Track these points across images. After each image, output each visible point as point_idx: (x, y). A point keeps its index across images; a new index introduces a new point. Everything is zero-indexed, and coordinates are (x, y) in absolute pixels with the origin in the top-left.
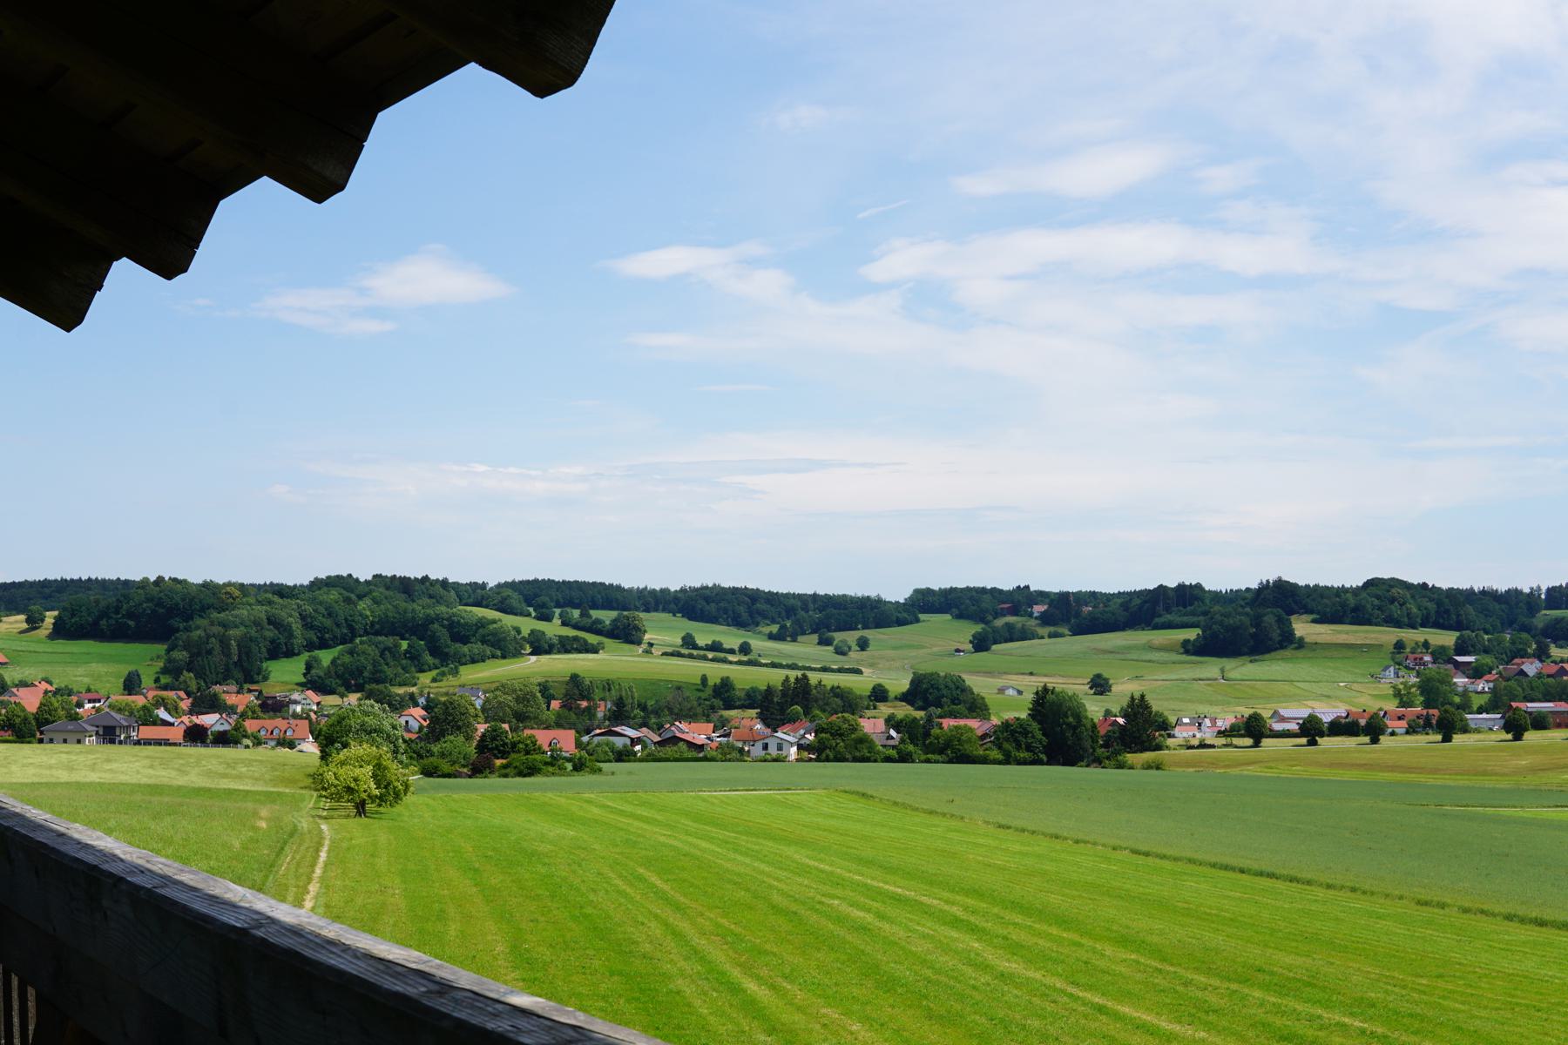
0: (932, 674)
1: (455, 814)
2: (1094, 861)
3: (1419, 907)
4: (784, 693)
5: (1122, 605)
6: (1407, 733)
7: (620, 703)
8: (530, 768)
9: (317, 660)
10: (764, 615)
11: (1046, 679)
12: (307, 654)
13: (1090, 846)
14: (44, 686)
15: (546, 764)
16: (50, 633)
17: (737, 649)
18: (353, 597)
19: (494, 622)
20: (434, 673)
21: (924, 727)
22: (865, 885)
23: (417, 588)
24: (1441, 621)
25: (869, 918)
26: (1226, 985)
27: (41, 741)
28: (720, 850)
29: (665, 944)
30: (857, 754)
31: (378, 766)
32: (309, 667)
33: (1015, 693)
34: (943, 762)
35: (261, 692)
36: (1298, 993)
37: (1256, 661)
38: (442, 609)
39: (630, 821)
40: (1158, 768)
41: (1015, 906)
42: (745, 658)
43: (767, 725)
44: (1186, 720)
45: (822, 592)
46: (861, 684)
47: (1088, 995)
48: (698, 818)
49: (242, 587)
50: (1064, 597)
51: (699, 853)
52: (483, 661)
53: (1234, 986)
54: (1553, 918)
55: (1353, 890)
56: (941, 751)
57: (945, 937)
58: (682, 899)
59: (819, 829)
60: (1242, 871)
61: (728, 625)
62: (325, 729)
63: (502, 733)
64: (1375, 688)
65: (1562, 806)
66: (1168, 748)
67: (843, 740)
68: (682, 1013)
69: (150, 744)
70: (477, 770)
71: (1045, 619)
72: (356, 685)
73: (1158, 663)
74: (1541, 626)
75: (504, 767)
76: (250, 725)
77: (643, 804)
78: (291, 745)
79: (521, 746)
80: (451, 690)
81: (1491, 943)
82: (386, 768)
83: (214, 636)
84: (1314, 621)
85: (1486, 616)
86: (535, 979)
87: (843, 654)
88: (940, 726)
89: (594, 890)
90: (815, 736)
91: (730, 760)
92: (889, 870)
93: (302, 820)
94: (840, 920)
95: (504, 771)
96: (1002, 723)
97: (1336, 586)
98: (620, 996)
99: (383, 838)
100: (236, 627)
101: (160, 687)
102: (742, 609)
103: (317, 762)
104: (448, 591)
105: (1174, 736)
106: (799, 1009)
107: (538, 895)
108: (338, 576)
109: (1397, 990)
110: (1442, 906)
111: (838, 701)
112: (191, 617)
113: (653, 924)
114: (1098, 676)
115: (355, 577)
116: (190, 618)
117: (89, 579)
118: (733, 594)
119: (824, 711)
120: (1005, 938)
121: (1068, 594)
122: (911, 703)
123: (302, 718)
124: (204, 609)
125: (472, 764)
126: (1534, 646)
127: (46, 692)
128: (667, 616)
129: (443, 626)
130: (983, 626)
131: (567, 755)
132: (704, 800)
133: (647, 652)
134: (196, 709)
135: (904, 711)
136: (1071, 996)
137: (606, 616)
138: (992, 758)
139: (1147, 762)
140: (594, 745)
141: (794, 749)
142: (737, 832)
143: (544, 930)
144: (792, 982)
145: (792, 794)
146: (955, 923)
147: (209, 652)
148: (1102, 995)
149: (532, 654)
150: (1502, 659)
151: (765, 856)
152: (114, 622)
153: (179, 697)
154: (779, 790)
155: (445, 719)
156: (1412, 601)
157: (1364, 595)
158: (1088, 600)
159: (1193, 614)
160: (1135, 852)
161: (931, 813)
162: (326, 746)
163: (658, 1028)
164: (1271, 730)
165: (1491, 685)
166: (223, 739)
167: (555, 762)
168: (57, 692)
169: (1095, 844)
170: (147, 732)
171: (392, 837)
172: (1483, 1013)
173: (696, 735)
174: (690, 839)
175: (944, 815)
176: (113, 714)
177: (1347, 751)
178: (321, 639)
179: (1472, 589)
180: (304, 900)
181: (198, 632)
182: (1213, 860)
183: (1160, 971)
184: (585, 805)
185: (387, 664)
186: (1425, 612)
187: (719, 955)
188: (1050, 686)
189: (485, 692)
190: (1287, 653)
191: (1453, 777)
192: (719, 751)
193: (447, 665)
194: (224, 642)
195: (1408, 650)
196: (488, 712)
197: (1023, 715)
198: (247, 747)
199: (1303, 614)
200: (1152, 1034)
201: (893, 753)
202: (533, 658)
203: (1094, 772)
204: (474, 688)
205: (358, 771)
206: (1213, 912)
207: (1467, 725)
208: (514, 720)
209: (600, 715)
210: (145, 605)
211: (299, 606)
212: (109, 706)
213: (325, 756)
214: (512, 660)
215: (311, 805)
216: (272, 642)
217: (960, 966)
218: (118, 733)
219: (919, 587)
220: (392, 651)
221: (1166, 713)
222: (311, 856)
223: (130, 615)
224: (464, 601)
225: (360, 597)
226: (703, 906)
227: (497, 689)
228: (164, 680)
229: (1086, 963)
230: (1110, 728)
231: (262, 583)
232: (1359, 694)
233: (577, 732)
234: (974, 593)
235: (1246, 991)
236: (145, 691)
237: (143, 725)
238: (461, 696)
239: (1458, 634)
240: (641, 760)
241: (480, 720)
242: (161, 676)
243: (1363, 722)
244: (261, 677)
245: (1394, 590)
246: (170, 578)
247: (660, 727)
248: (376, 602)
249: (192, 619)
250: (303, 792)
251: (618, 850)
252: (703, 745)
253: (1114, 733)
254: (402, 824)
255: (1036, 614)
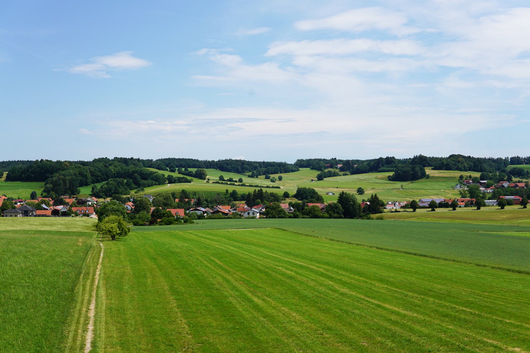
0: (304, 188)
1: (145, 238)
2: (365, 252)
3: (477, 267)
4: (254, 195)
5: (367, 164)
6: (465, 207)
7: (199, 199)
8: (169, 222)
9: (95, 186)
10: (246, 169)
11: (343, 190)
12: (92, 185)
13: (362, 246)
14: (4, 197)
15: (175, 220)
16: (5, 179)
17: (238, 181)
18: (108, 165)
19: (155, 173)
20: (136, 190)
21: (302, 206)
22: (289, 262)
23: (129, 162)
24: (475, 169)
25: (293, 274)
26: (420, 296)
27: (3, 216)
28: (237, 250)
29: (224, 285)
30: (280, 216)
31: (119, 223)
32: (93, 189)
33: (332, 194)
34: (309, 218)
35: (77, 198)
36: (445, 299)
37: (413, 183)
38: (138, 168)
39: (205, 240)
40: (381, 219)
41: (342, 268)
42: (241, 184)
43: (249, 206)
44: (390, 203)
45: (266, 161)
46: (280, 192)
47: (373, 301)
48: (229, 238)
49: (70, 162)
50: (348, 161)
51: (230, 251)
52: (152, 186)
53: (423, 297)
54: (524, 270)
55: (454, 261)
56: (308, 214)
57: (320, 280)
58: (228, 268)
59: (270, 242)
60: (415, 255)
61: (235, 173)
62: (99, 210)
63: (159, 210)
64: (453, 192)
65: (519, 231)
66: (384, 212)
67: (275, 211)
68: (233, 310)
69: (40, 216)
70: (152, 223)
71: (342, 169)
72: (109, 195)
73: (380, 183)
74: (509, 170)
75: (160, 222)
76: (74, 209)
77: (209, 234)
78: (88, 215)
79: (166, 215)
80: (142, 196)
81: (505, 279)
82: (122, 224)
83: (61, 179)
84: (432, 169)
85: (490, 167)
86: (180, 299)
87: (274, 182)
88: (307, 206)
89: (197, 266)
90: (265, 210)
91: (237, 218)
92: (297, 256)
93: (94, 242)
94: (283, 274)
95: (160, 223)
96: (328, 204)
97: (439, 157)
98: (210, 304)
99: (122, 248)
100: (68, 176)
101: (43, 197)
102: (239, 167)
103: (97, 221)
104: (140, 163)
105: (386, 208)
106: (274, 308)
107: (177, 268)
108: (102, 158)
109: (478, 297)
110: (485, 266)
111: (273, 198)
112: (53, 173)
113: (219, 277)
114: (360, 188)
115: (108, 158)
116: (52, 173)
117: (18, 161)
118: (236, 162)
119: (268, 201)
120: (340, 280)
121: (349, 160)
122: (297, 198)
123: (91, 206)
124: (57, 170)
125: (150, 221)
126: (507, 177)
127: (4, 199)
128: (214, 170)
129: (139, 175)
130: (321, 172)
131: (182, 217)
132: (229, 232)
133: (208, 182)
134: (55, 204)
135: (295, 201)
136: (367, 301)
137: (193, 170)
138: (325, 216)
139: (378, 217)
140: (190, 214)
141: (258, 214)
142: (242, 243)
143: (181, 280)
144: (270, 298)
145: (260, 230)
146: (322, 275)
147: (59, 185)
148: (378, 300)
149: (169, 183)
150: (496, 182)
151: (253, 252)
152: (27, 175)
153: (49, 200)
154: (255, 228)
155: (140, 206)
156: (465, 162)
157: (449, 160)
158: (356, 163)
159: (392, 167)
160: (377, 248)
161: (307, 235)
162: (100, 216)
163: (225, 316)
164: (419, 206)
165: (492, 190)
166: (65, 214)
167: (178, 220)
168: (8, 199)
169: (364, 245)
170: (39, 212)
171: (125, 248)
172: (510, 305)
173: (225, 210)
174: (227, 246)
175: (311, 236)
176: (27, 206)
177: (445, 213)
178: (97, 179)
179: (485, 158)
180: (96, 271)
181: (55, 178)
182: (405, 251)
183: (396, 291)
184: (189, 235)
185: (120, 188)
186: (470, 166)
187: (243, 288)
188: (345, 192)
189: (153, 196)
190: (423, 180)
191: (481, 221)
192: (233, 215)
193: (140, 188)
194: (64, 181)
195: (464, 179)
196: (155, 203)
197: (335, 202)
198: (73, 216)
199: (429, 167)
200: (398, 315)
201: (292, 215)
202: (169, 185)
203: (359, 221)
204: (149, 195)
205: (112, 225)
206: (409, 269)
207: (485, 204)
208: (163, 206)
209: (192, 203)
210: (37, 169)
211: (89, 169)
212: (26, 204)
213: (100, 220)
214: (162, 185)
215: (96, 236)
216: (81, 181)
217: (327, 291)
218: (29, 213)
219: (299, 159)
220: (122, 183)
221: (383, 201)
222: (98, 255)
223: (32, 173)
224: (145, 166)
225: (110, 165)
226: (235, 270)
227: (157, 195)
228: (44, 194)
229: (370, 289)
230: (365, 206)
231: (77, 161)
232: (448, 194)
233: (184, 209)
234: (318, 161)
235: (427, 298)
236: (38, 198)
237: (38, 210)
238: (145, 198)
239: (481, 173)
240: (207, 219)
241: (152, 206)
242: (43, 193)
243: (450, 203)
244: (77, 193)
245: (459, 159)
246: (45, 160)
247: (213, 207)
248: (115, 166)
249: (53, 173)
250: (93, 232)
251: (203, 250)
252: (227, 213)
253: (366, 207)
254: (128, 243)
255: (338, 168)
